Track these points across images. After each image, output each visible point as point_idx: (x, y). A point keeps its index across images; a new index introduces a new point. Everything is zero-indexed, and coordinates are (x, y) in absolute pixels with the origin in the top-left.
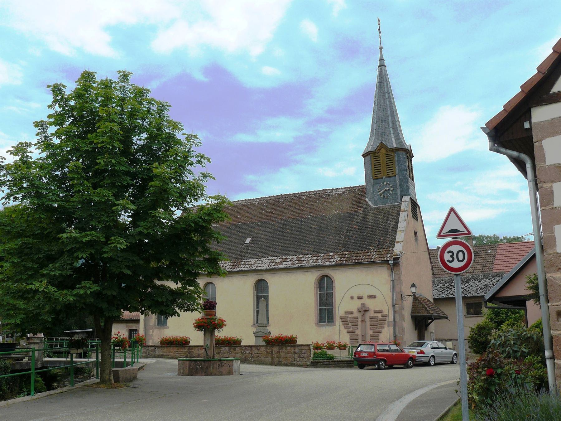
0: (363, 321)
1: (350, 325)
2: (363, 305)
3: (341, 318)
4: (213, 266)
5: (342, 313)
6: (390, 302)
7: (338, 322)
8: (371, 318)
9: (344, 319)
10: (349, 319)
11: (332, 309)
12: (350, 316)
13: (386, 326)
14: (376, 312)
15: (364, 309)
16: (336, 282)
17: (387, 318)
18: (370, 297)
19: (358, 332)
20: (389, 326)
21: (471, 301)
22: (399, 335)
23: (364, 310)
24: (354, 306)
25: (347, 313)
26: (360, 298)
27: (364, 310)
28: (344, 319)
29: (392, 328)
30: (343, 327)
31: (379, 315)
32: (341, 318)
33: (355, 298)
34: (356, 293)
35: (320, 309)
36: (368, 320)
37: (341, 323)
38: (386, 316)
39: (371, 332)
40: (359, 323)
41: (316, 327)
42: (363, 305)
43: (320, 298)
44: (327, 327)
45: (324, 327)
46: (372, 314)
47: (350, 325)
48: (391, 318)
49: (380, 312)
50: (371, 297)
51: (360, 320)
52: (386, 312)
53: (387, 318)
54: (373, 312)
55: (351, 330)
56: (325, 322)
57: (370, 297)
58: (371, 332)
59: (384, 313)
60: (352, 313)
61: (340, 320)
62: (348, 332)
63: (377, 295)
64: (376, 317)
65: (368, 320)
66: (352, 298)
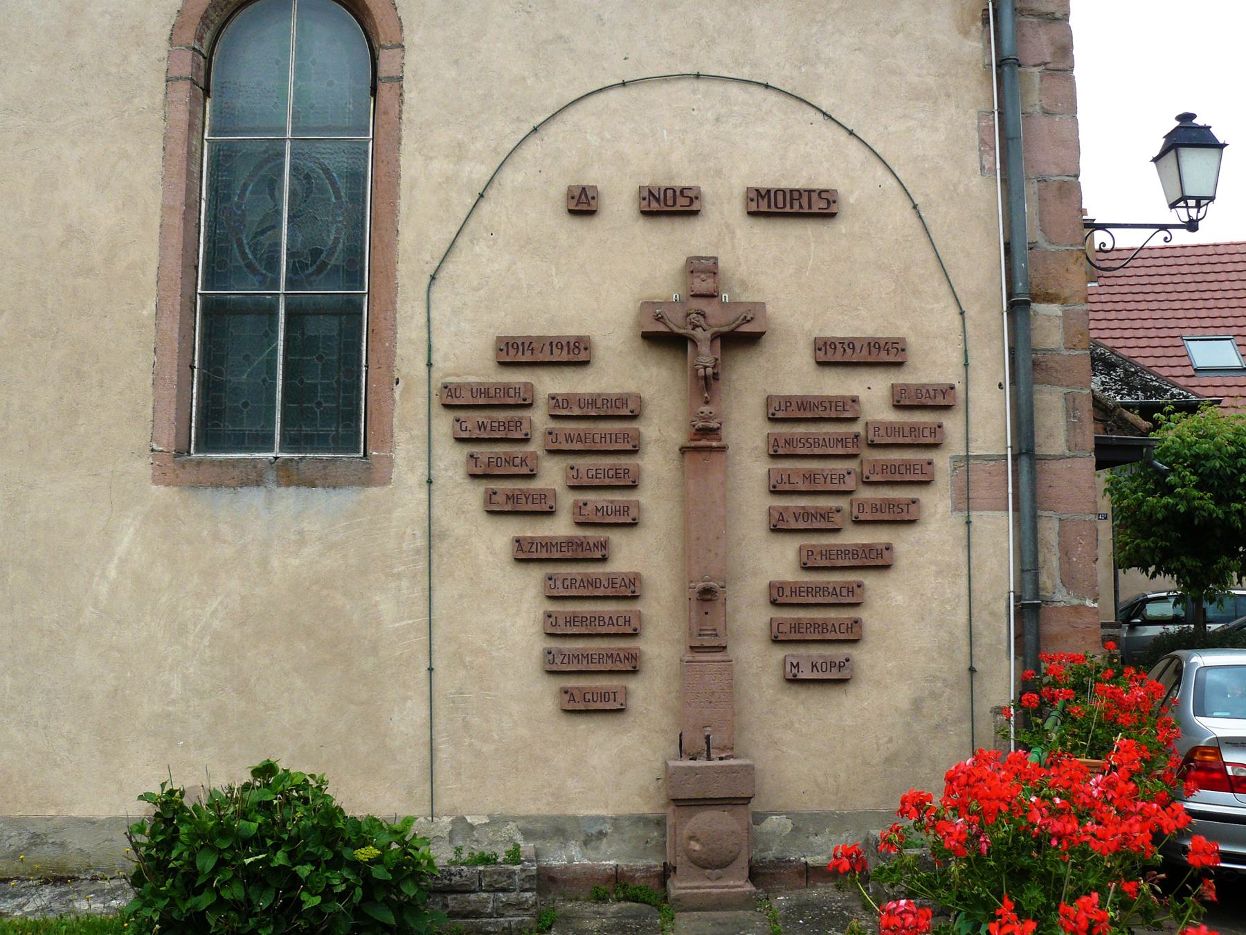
0: (704, 442)
1: (552, 475)
2: (703, 272)
3: (454, 400)
4: (205, 829)
5: (466, 355)
6: (981, 268)
7: (416, 448)
8: (783, 412)
9: (486, 421)
10: (539, 419)
11: (350, 311)
12: (549, 384)
13: (937, 504)
14: (833, 355)
15: (719, 319)
16: (414, 36)
17: (952, 424)
18: (776, 205)
19: (643, 554)
20: (965, 502)
21: (1102, 442)
22: (1062, 597)
23: (702, 335)
24: (605, 286)
25: (516, 353)
26: (669, 205)
27: (702, 335)
28: (486, 421)
29: (997, 531)
30: (474, 495)
31: (872, 393)
32: (454, 400)
33: (619, 203)
34: (627, 148)
35: (215, 312)
36: (747, 432)
37: (452, 460)
38: (939, 400)
39: (779, 561)
40: (657, 464)
41: (161, 493)
42: (703, 272)
43: (219, 194)
44: (289, 499)
45: (254, 497)
46: (789, 371)
47: (552, 475)
48: (986, 424)
49: (884, 355)
50: (791, 205)
51: (662, 432)
52: (933, 365)
53: (952, 424)
54: (803, 358)
55: (560, 527)
56: (265, 442)
57: (776, 205)
58: (779, 561)
59: (505, 533)
60: (574, 354)
61: (444, 424)
62: (526, 555)
63: (851, 197)
64: (841, 411)
65: (747, 432)
66: (583, 205)
